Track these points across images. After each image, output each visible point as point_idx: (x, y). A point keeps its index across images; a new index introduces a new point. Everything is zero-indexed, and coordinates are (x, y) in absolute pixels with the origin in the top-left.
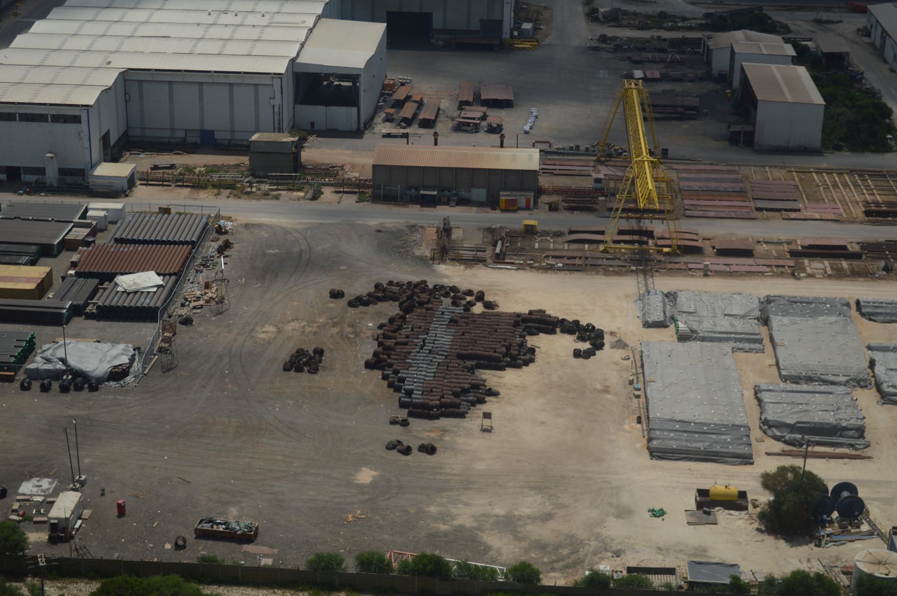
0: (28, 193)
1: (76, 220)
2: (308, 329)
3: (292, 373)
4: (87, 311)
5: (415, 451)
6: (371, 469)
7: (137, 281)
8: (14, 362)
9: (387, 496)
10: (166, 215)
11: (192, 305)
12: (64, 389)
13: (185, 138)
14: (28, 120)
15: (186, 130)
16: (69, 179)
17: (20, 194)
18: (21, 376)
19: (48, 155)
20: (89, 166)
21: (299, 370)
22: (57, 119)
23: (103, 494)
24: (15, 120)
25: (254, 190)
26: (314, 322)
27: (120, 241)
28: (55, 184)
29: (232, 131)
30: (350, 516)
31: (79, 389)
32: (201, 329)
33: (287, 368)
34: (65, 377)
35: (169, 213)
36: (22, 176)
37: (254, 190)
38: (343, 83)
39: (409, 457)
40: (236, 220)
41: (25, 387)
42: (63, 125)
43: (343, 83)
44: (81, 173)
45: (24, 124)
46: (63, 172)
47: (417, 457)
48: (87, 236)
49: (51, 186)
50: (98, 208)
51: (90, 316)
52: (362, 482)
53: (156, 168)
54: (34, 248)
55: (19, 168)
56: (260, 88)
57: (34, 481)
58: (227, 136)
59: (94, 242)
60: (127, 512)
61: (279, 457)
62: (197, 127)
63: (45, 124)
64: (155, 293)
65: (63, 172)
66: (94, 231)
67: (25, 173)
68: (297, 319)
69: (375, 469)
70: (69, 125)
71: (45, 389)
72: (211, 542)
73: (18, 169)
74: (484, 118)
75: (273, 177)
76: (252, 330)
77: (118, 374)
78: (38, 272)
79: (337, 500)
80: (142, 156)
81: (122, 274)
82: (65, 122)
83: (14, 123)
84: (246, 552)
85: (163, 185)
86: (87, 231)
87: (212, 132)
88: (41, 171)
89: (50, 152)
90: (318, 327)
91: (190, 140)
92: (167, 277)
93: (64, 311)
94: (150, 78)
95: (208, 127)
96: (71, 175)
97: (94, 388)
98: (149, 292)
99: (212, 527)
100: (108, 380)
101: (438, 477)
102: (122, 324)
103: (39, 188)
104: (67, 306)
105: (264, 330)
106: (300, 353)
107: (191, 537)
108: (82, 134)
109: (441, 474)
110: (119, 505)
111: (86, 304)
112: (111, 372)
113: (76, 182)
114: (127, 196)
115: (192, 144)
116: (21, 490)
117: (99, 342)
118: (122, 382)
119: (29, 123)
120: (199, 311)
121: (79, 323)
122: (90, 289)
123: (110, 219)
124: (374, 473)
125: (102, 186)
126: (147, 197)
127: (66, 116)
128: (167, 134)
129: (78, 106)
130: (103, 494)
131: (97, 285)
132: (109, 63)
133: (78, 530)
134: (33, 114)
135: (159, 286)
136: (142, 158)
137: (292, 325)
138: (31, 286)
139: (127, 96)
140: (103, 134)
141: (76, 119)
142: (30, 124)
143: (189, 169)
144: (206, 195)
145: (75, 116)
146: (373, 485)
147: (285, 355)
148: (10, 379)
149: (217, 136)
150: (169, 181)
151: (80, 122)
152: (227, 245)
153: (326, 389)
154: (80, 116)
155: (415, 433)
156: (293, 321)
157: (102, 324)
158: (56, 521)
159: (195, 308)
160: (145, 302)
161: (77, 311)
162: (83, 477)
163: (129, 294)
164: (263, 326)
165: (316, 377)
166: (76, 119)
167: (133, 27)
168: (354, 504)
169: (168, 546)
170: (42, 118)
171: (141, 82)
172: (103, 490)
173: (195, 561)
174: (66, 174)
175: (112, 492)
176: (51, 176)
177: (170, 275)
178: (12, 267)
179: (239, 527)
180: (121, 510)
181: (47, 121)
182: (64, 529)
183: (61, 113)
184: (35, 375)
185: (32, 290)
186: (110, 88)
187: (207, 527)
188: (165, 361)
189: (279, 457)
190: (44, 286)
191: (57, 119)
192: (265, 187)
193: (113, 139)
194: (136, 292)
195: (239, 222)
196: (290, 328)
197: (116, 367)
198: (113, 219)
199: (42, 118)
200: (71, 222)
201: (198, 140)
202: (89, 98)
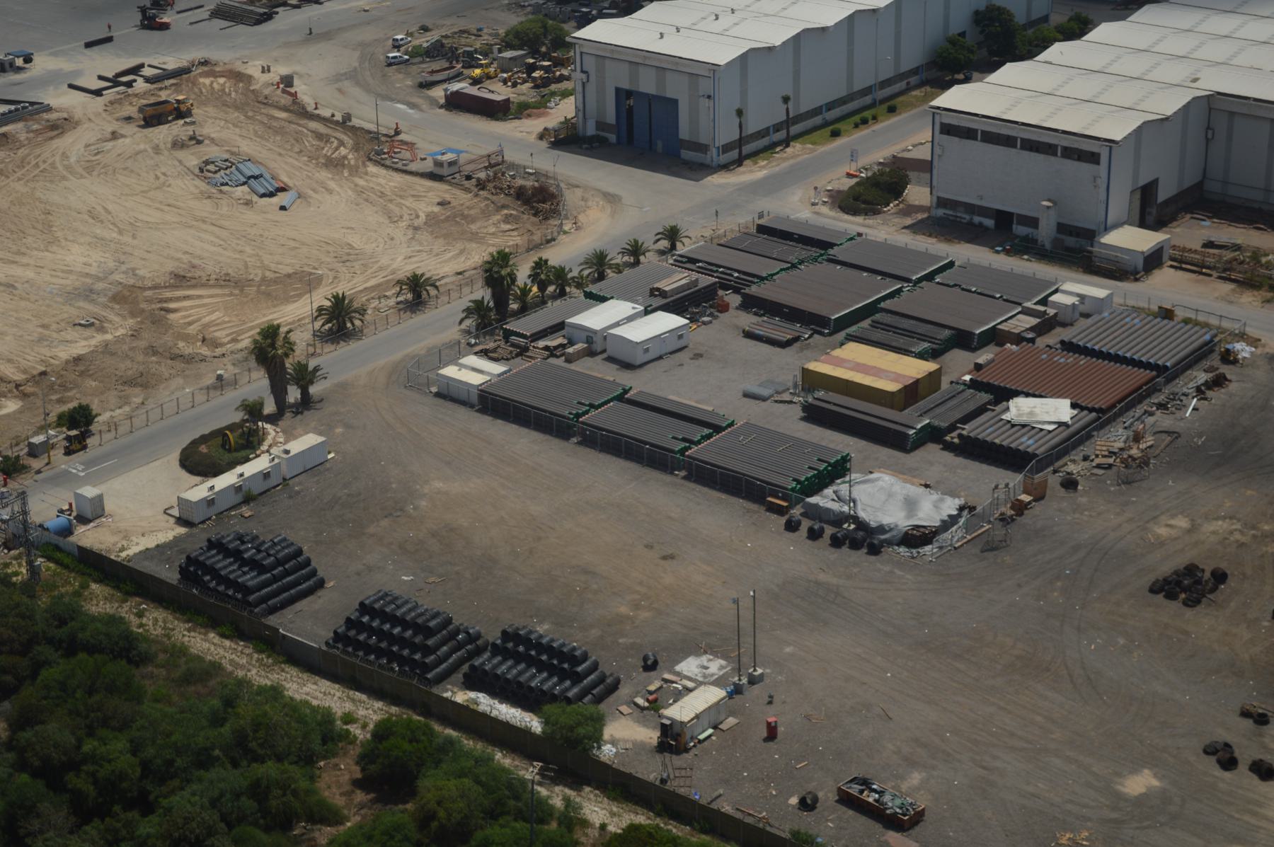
0: (1008, 253)
1: (1028, 304)
2: (1237, 536)
3: (1160, 598)
4: (948, 438)
5: (1243, 768)
6: (1155, 776)
7: (1037, 410)
8: (793, 490)
9: (1146, 823)
10: (1166, 321)
11: (1097, 461)
12: (836, 542)
14: (1031, 150)
16: (1071, 241)
17: (998, 252)
18: (797, 512)
20: (1102, 227)
21: (1171, 596)
23: (770, 703)
26: (1254, 528)
27: (1068, 346)
30: (118, 745)
31: (855, 545)
32: (1083, 500)
33: (1153, 590)
34: (846, 526)
39: (1227, 775)
40: (1264, 346)
41: (792, 526)
42: (1076, 163)
45: (1026, 153)
46: (1062, 228)
47: (1243, 779)
48: (1032, 329)
50: (1073, 288)
51: (948, 447)
52: (1126, 790)
53: (1210, 244)
54: (947, 333)
55: (1011, 214)
57: (704, 659)
59: (1032, 341)
60: (780, 736)
61: (1039, 719)
63: (1053, 158)
64: (1050, 432)
65: (1062, 228)
66: (1047, 324)
67: (1018, 223)
68: (1231, 518)
69: (1160, 779)
70: (1084, 165)
71: (814, 535)
72: (851, 812)
76: (1155, 518)
77: (917, 538)
78: (915, 368)
79: (1069, 807)
80: (1207, 223)
81: (1027, 395)
82: (1079, 159)
83: (1014, 150)
84: (887, 842)
85: (1181, 269)
86: (1034, 321)
88: (1033, 222)
89: (1049, 200)
90: (1254, 536)
92: (1085, 412)
93: (911, 432)
94: (1245, 111)
96: (1078, 235)
97: (874, 550)
98: (1042, 430)
99: (862, 792)
100: (898, 545)
101: (1247, 818)
102: (985, 467)
103: (1027, 248)
104: (919, 426)
105: (1172, 522)
106: (1191, 570)
107: (827, 795)
108: (1099, 181)
109: (1255, 814)
110: (769, 724)
111: (952, 428)
112: (906, 533)
113: (1076, 248)
114: (1137, 280)
116: (678, 668)
117: (927, 486)
118: (914, 551)
119: (1033, 154)
120: (1101, 472)
121: (932, 451)
122: (971, 406)
124: (1155, 783)
125: (1108, 260)
129: (1098, 139)
130: (770, 703)
131: (989, 403)
133: (700, 742)
135: (1061, 424)
136: (1203, 227)
137: (1220, 525)
138: (892, 387)
139: (1210, 132)
140: (1142, 183)
141: (1093, 158)
144: (1250, 299)
145: (1093, 154)
146: (1140, 801)
147: (1167, 567)
148: (780, 511)
150: (1209, 268)
151: (1098, 163)
152: (1219, 381)
153: (1187, 633)
154: (1099, 155)
155: (1266, 740)
156: (1224, 518)
157: (960, 461)
158: (668, 722)
159: (1099, 466)
160: (1026, 443)
161: (933, 435)
162: (760, 671)
163: (1013, 426)
164: (1173, 516)
165: (1189, 613)
166: (1093, 158)
168: (1089, 819)
169: (794, 801)
171: (1232, 114)
172: (771, 697)
173: (786, 835)
175: (784, 702)
176: (1046, 232)
177: (1091, 410)
178: (892, 356)
179: (892, 804)
180: (772, 733)
181: (1055, 154)
182: (677, 737)
183: (1076, 146)
184: (815, 513)
185: (893, 393)
186: (1167, 119)
187: (854, 789)
188: (993, 534)
189: (1039, 719)
190: (912, 393)
193: (1163, 194)
194: (1024, 426)
195: (1267, 350)
196: (1212, 528)
197: (917, 527)
198: (1086, 309)
200: (1020, 304)
202: (1118, 129)
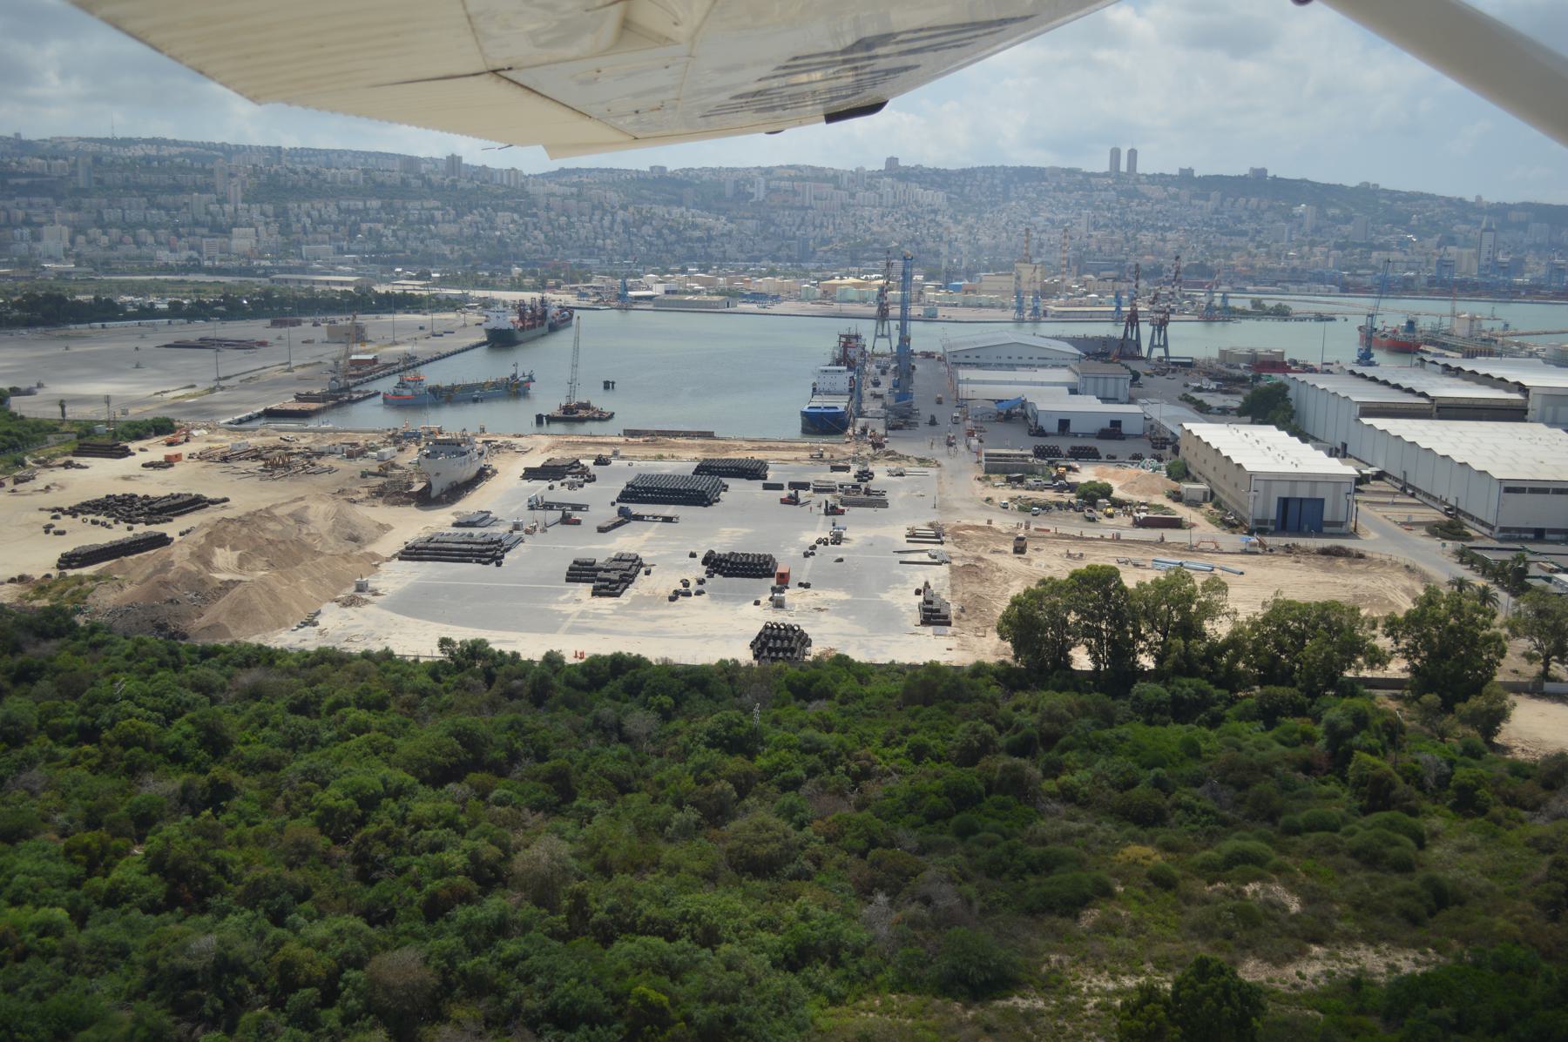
46: (1257, 521)
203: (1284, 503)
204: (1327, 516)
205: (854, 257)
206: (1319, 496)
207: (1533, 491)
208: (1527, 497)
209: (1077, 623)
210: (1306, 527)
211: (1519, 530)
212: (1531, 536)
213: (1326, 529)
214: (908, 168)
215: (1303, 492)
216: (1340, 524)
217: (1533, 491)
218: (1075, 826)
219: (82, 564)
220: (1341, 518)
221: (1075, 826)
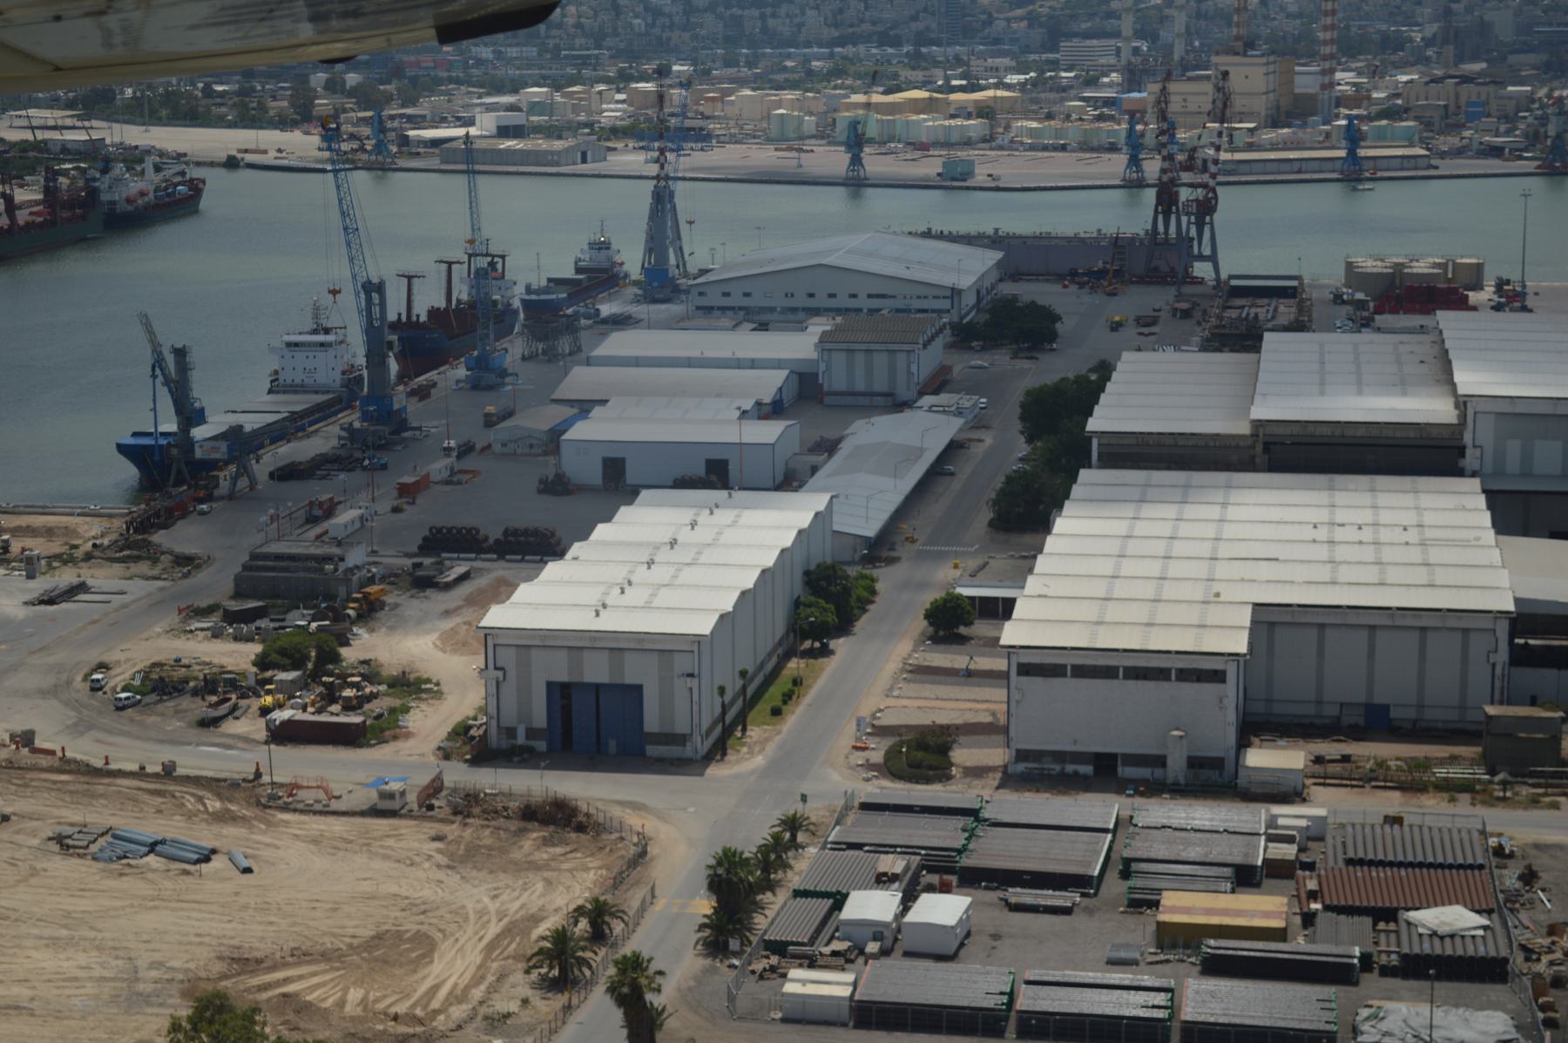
13: (1338, 718)
14: (1137, 677)
15: (1342, 705)
17: (1129, 796)
19: (1175, 733)
22: (1186, 675)
24: (1116, 677)
25: (1508, 794)
28: (1182, 781)
29: (1420, 707)
35: (1401, 824)
36: (1120, 769)
37: (1508, 794)
38: (1531, 642)
42: (1197, 686)
43: (1531, 642)
44: (1217, 763)
45: (1131, 683)
46: (1194, 763)
49: (1176, 784)
56: (1473, 636)
58: (1411, 714)
62: (1362, 699)
63: (1166, 684)
65: (1194, 763)
67: (1124, 764)
70: (1206, 686)
73: (1112, 757)
74: (1301, 850)
75: (1542, 775)
82: (1199, 680)
83: (1115, 682)
87: (1386, 708)
88: (1160, 761)
91: (1347, 720)
94: (1288, 619)
95: (1379, 699)
108: (1226, 701)
115: (1350, 726)
119: (1140, 683)
123: (1312, 833)
126: (1322, 805)
127: (1199, 671)
128: (1310, 710)
132: (1217, 595)
134: (1147, 669)
141: (1218, 677)
142: (1141, 684)
143: (1381, 764)
145: (1216, 672)
149: (1394, 713)
151: (1223, 681)
166: (1218, 677)
167: (672, 570)
170: (1161, 674)
174: (1201, 766)
176: (1177, 766)
191: (1186, 675)
192: (1525, 791)
199: (1161, 674)
201: (1361, 721)
203: (562, 694)
204: (651, 723)
205: (235, 74)
206: (629, 680)
207: (1081, 672)
208: (1069, 684)
209: (122, 93)
210: (612, 745)
211: (1060, 756)
212: (1087, 769)
213: (652, 750)
214: (254, 431)
215: (596, 672)
216: (681, 739)
217: (1081, 672)
218: (84, 904)
219: (1534, 634)
220: (681, 727)
221: (84, 904)
